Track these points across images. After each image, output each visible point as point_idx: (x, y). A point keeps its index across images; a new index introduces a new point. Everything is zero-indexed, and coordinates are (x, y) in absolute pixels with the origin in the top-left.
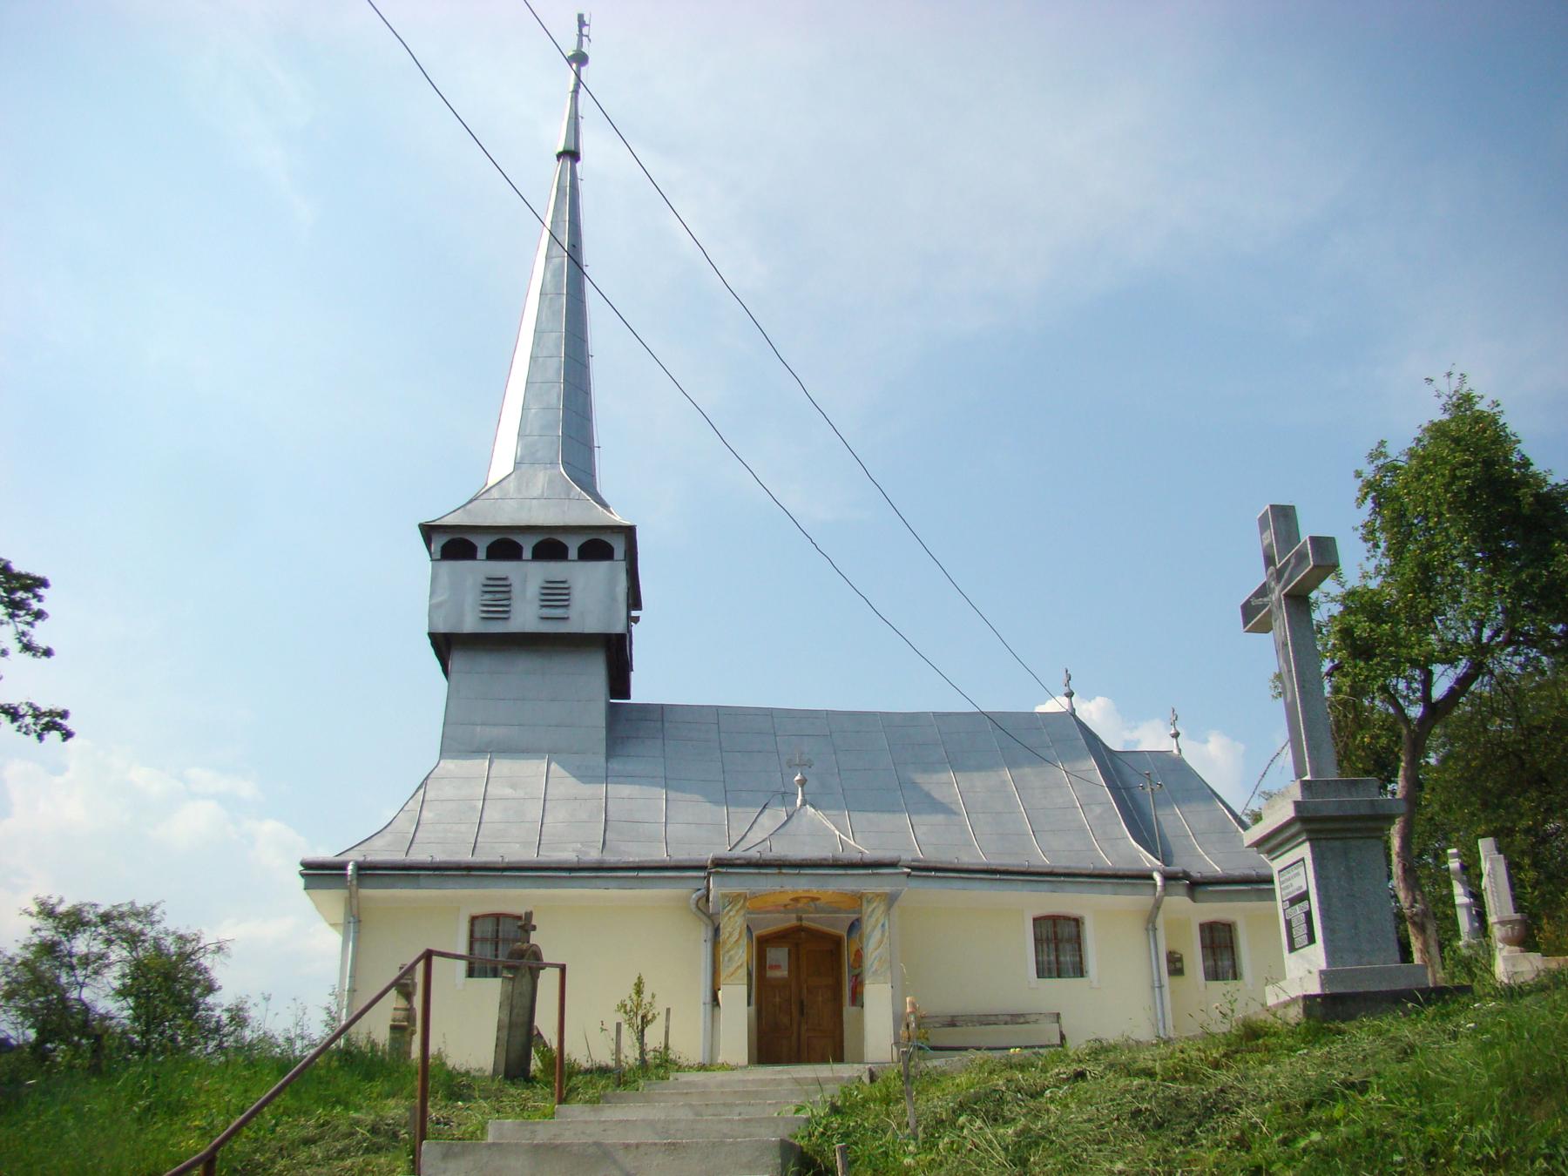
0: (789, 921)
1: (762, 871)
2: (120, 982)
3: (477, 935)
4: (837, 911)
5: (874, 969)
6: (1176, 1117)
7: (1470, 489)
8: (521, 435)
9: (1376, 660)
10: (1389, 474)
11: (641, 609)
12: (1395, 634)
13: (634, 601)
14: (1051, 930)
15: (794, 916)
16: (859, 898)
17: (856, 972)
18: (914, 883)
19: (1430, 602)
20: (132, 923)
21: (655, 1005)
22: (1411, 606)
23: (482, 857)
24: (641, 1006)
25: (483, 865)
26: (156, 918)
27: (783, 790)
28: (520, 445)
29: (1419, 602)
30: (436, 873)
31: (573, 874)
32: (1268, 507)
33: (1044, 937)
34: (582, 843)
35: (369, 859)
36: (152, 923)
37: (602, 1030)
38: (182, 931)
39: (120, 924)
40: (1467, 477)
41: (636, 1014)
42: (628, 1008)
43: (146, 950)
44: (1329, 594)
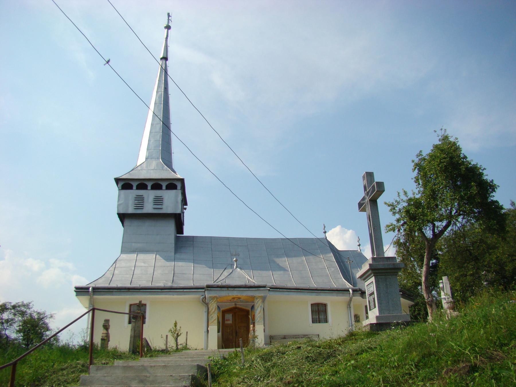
0: (232, 305)
1: (222, 289)
2: (18, 328)
3: (132, 310)
4: (248, 302)
5: (258, 320)
6: (319, 358)
7: (445, 166)
8: (148, 149)
9: (417, 221)
10: (423, 161)
11: (187, 205)
12: (423, 212)
13: (184, 202)
14: (317, 308)
15: (234, 303)
16: (253, 298)
17: (254, 322)
18: (271, 293)
19: (434, 202)
20: (23, 309)
21: (181, 330)
22: (429, 203)
23: (134, 285)
24: (176, 330)
25: (133, 288)
26: (30, 307)
27: (231, 263)
28: (147, 152)
29: (431, 202)
30: (119, 290)
31: (162, 291)
32: (365, 173)
33: (315, 310)
34: (166, 281)
35: (97, 286)
36: (29, 308)
37: (162, 337)
38: (39, 311)
39: (19, 309)
40: (444, 162)
41: (175, 333)
42: (172, 331)
43: (27, 317)
44: (403, 199)
